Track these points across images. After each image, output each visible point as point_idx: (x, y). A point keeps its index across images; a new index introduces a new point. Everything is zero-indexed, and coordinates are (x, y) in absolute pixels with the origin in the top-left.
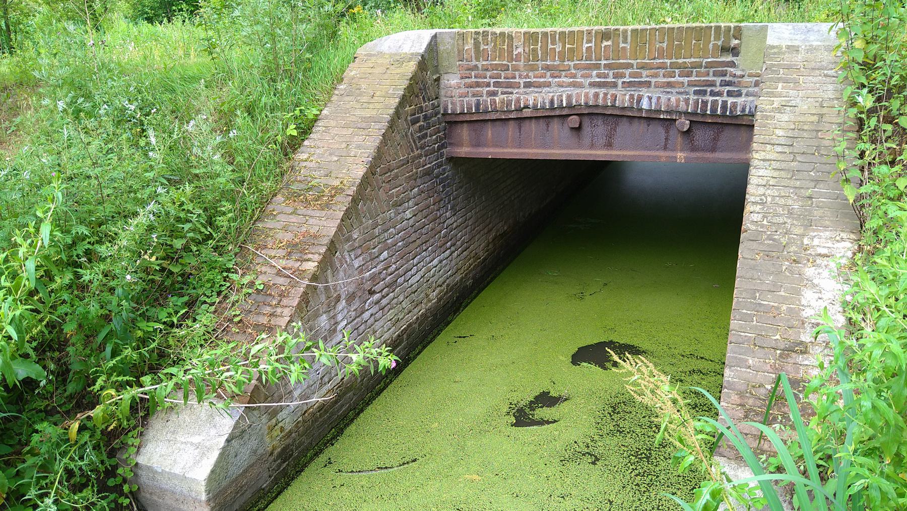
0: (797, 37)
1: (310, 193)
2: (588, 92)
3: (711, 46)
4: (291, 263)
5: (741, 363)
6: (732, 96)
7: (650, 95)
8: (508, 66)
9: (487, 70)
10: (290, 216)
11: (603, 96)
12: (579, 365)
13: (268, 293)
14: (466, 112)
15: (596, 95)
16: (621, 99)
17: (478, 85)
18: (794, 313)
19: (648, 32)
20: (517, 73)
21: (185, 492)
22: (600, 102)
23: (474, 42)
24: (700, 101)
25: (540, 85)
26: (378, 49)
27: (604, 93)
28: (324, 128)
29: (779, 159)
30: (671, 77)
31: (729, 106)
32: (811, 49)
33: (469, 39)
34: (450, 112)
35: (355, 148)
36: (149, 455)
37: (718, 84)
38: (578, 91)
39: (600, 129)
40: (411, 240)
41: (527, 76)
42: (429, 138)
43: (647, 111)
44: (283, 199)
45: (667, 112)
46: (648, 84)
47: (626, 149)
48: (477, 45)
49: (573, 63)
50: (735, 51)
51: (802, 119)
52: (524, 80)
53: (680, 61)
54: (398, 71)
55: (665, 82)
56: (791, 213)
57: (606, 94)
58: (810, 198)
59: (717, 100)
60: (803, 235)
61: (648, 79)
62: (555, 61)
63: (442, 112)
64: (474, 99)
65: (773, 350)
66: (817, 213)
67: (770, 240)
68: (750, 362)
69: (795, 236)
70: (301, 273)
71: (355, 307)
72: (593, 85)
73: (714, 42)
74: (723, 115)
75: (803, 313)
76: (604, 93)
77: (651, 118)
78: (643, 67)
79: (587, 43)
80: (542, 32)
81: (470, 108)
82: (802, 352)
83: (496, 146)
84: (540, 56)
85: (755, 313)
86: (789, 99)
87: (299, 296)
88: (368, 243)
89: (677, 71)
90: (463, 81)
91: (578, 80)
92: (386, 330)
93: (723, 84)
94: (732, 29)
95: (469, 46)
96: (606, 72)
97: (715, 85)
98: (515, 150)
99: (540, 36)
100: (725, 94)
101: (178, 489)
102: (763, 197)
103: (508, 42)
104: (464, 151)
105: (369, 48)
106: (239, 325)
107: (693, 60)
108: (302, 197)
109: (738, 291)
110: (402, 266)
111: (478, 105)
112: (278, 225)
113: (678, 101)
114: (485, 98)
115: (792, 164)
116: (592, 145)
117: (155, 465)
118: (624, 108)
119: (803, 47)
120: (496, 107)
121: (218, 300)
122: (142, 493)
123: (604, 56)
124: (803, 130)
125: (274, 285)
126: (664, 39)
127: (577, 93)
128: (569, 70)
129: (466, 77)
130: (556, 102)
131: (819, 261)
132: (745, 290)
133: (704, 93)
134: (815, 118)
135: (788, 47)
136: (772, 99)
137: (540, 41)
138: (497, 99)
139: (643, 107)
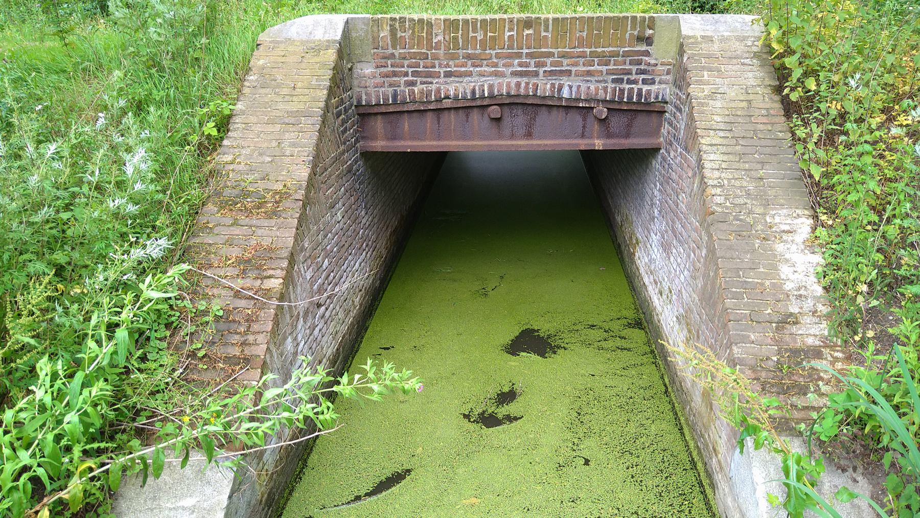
0: (708, 28)
1: (249, 200)
2: (510, 82)
3: (627, 35)
4: (248, 283)
5: (745, 339)
6: (646, 84)
7: (570, 84)
8: (428, 54)
9: (404, 58)
10: (231, 228)
11: (525, 86)
12: (519, 355)
13: (230, 319)
14: (382, 103)
15: (518, 85)
16: (542, 88)
17: (395, 74)
18: (777, 287)
19: (569, 21)
22: (522, 91)
23: (391, 29)
24: (618, 89)
25: (461, 75)
26: (284, 35)
27: (526, 83)
28: (243, 125)
29: (724, 143)
30: (591, 66)
31: (644, 93)
32: (723, 40)
33: (385, 26)
34: (364, 103)
35: (289, 146)
37: (634, 72)
39: (520, 119)
41: (448, 66)
42: (348, 132)
43: (567, 99)
44: (216, 209)
46: (568, 73)
47: (545, 138)
48: (393, 31)
49: (495, 52)
50: (649, 41)
51: (733, 105)
52: (445, 69)
53: (599, 50)
54: (317, 59)
55: (584, 71)
56: (748, 194)
57: (527, 84)
59: (633, 88)
60: (764, 214)
61: (568, 68)
62: (476, 49)
63: (355, 104)
65: (768, 324)
66: (772, 193)
67: (737, 220)
68: (753, 337)
69: (758, 216)
70: (267, 293)
71: (309, 325)
72: (514, 74)
74: (639, 103)
75: (785, 286)
76: (526, 83)
77: (570, 107)
78: (564, 56)
79: (509, 31)
80: (462, 20)
83: (413, 138)
84: (461, 44)
85: (744, 290)
86: (716, 86)
87: (272, 319)
88: (315, 251)
89: (596, 59)
90: (379, 71)
91: (500, 69)
92: (329, 345)
93: (638, 72)
94: (647, 20)
95: (385, 33)
96: (528, 60)
97: (631, 74)
98: (435, 143)
99: (461, 24)
100: (640, 82)
102: (720, 180)
103: (427, 28)
104: (380, 145)
105: (273, 34)
106: (205, 360)
107: (611, 49)
108: (239, 205)
109: (723, 271)
111: (395, 96)
112: (220, 240)
113: (597, 89)
114: (402, 88)
115: (737, 148)
116: (513, 135)
118: (545, 97)
119: (716, 37)
120: (415, 97)
123: (526, 45)
124: (737, 115)
125: (235, 309)
126: (584, 28)
127: (499, 83)
128: (491, 58)
129: (382, 66)
130: (477, 92)
132: (729, 270)
133: (620, 81)
134: (744, 104)
135: (703, 37)
136: (702, 86)
137: (460, 29)
138: (416, 89)
139: (564, 96)
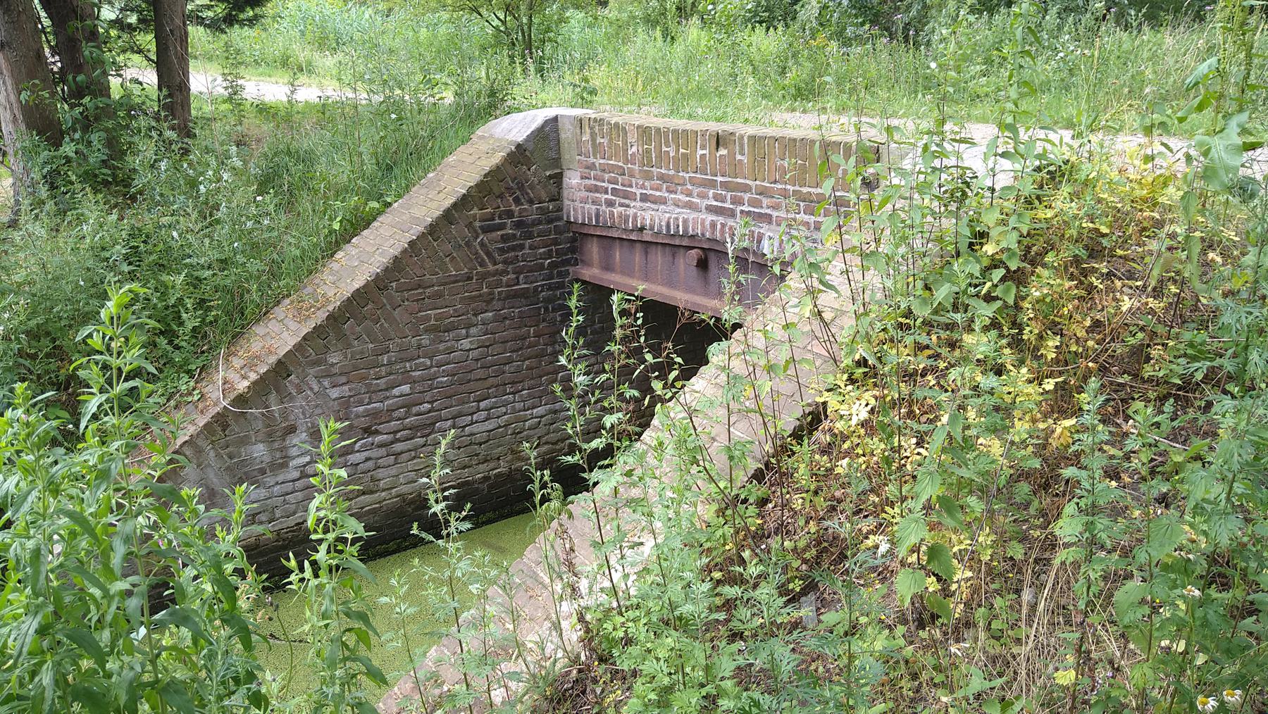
20: (633, 180)
40: (472, 376)
53: (805, 190)
61: (768, 211)
64: (594, 207)
72: (710, 209)
78: (763, 192)
110: (446, 408)
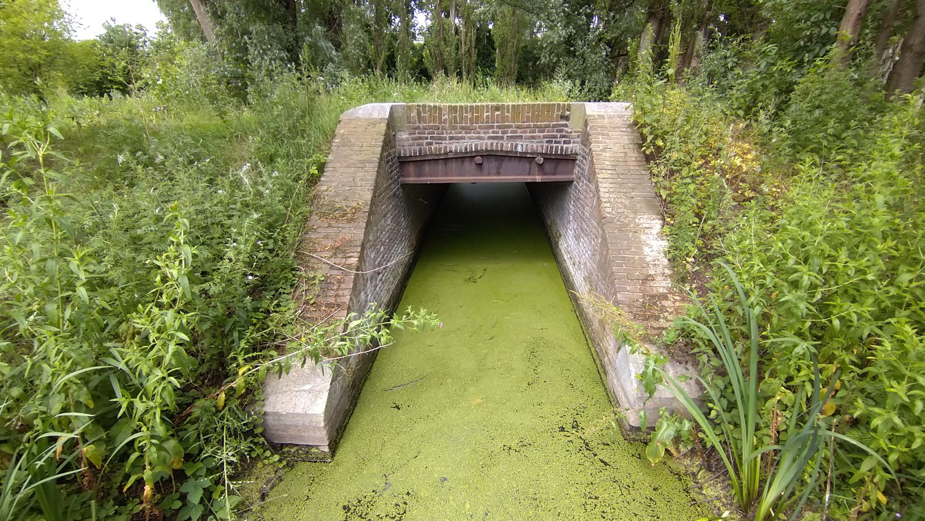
4: (338, 260)
5: (624, 290)
9: (426, 129)
11: (496, 145)
15: (492, 144)
17: (420, 138)
18: (642, 260)
21: (307, 424)
22: (494, 148)
25: (458, 138)
32: (610, 117)
36: (272, 404)
38: (481, 142)
39: (492, 164)
41: (451, 133)
45: (531, 153)
46: (521, 137)
48: (419, 113)
50: (567, 118)
53: (539, 124)
54: (375, 130)
56: (625, 207)
57: (497, 144)
58: (632, 198)
60: (634, 218)
66: (638, 206)
70: (349, 266)
72: (490, 138)
73: (556, 113)
78: (518, 127)
81: (415, 153)
82: (652, 280)
90: (411, 136)
101: (301, 423)
104: (412, 180)
111: (420, 151)
113: (537, 147)
117: (280, 411)
118: (507, 152)
121: (292, 290)
122: (269, 432)
131: (646, 231)
135: (598, 116)
